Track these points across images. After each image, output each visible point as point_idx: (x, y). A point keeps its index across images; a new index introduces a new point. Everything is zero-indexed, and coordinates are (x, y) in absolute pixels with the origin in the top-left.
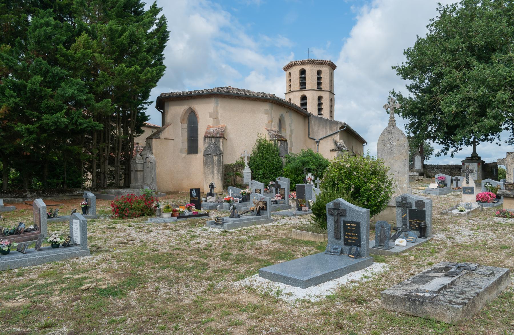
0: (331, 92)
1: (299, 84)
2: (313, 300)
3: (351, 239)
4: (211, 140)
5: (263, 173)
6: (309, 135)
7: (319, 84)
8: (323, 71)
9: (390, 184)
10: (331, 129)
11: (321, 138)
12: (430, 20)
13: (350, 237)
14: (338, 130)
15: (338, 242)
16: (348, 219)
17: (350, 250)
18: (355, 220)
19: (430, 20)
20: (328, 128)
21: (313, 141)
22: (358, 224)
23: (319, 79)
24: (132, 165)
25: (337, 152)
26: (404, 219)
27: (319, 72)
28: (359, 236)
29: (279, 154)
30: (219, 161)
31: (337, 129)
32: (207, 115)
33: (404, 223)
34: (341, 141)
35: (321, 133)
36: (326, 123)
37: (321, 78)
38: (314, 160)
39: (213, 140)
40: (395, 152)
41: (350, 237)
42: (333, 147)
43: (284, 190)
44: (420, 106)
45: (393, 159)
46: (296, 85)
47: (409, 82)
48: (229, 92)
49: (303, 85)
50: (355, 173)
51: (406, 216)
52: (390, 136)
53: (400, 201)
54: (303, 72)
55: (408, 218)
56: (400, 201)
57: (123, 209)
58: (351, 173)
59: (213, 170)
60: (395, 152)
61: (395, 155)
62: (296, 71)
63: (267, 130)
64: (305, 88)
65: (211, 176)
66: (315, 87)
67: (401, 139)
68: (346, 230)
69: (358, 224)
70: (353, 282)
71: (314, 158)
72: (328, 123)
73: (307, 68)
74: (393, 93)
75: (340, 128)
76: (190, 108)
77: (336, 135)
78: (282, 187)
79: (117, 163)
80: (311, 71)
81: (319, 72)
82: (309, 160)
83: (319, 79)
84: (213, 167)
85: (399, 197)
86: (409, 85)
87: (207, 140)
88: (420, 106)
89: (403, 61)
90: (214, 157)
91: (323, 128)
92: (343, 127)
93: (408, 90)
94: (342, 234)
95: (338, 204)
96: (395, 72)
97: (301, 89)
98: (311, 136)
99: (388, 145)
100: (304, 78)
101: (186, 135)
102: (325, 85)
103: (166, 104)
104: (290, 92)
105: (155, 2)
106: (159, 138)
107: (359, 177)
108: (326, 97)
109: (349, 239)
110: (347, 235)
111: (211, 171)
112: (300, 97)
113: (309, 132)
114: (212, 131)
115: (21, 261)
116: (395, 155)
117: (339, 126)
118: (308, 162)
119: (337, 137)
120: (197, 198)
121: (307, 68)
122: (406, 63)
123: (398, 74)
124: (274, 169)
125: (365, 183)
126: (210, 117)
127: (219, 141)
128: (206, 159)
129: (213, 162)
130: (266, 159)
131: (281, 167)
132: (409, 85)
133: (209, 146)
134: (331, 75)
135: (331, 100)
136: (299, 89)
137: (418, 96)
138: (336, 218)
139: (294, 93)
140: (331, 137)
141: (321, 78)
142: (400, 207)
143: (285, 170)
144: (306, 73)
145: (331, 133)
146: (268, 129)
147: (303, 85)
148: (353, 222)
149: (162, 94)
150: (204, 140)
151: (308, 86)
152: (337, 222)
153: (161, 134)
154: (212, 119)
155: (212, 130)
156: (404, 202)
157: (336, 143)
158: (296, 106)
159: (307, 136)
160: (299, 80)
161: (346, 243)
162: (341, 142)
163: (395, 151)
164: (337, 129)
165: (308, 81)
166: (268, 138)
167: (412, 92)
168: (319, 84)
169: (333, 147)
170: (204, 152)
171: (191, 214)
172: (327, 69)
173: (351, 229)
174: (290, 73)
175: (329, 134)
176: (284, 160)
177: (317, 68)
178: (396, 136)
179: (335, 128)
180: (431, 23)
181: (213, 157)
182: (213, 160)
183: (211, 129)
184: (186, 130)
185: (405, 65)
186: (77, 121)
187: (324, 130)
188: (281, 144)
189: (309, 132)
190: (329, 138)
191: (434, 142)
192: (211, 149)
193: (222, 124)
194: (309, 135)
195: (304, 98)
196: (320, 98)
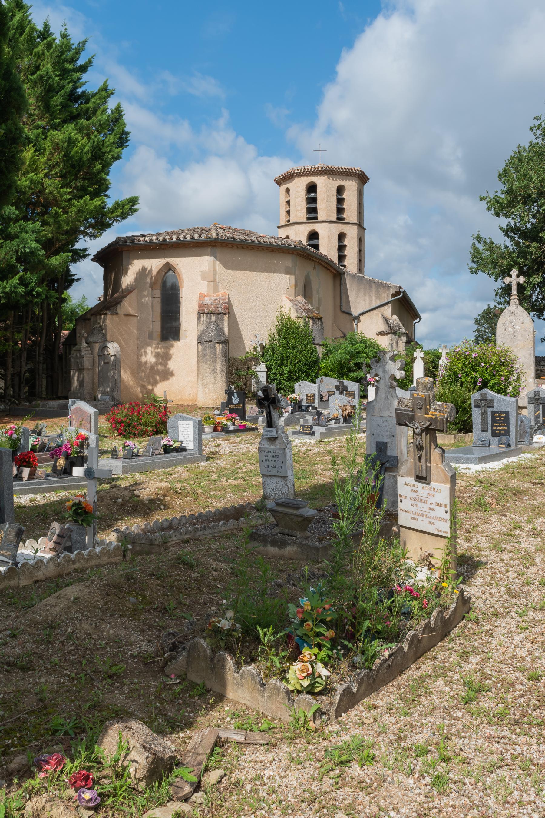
0: (360, 226)
1: (304, 211)
2: (491, 470)
3: (499, 430)
4: (210, 318)
5: (288, 372)
6: (341, 308)
7: (340, 210)
8: (347, 188)
9: (518, 377)
10: (378, 297)
11: (361, 311)
12: (536, 119)
13: (499, 428)
14: (390, 299)
15: (484, 434)
16: (495, 409)
17: (500, 440)
18: (504, 410)
19: (536, 119)
20: (373, 295)
21: (347, 316)
22: (507, 413)
23: (340, 201)
24: (72, 360)
25: (389, 336)
26: (537, 417)
27: (340, 190)
28: (508, 426)
29: (313, 339)
30: (226, 353)
31: (387, 296)
32: (196, 275)
33: (537, 422)
34: (395, 317)
35: (362, 303)
36: (370, 287)
37: (344, 199)
38: (367, 350)
39: (213, 318)
40: (519, 338)
41: (499, 428)
42: (382, 327)
43: (354, 394)
44: (522, 260)
45: (516, 347)
46: (299, 210)
47: (504, 221)
48: (233, 238)
49: (312, 212)
50: (483, 365)
51: (539, 414)
52: (512, 318)
53: (533, 396)
54: (312, 188)
55: (541, 416)
56: (533, 396)
57: (129, 425)
58: (478, 365)
59: (215, 367)
60: (519, 338)
61: (518, 342)
62: (299, 187)
63: (291, 301)
64: (316, 218)
65: (211, 376)
66: (334, 217)
67: (525, 322)
68: (494, 420)
69: (507, 413)
70: (513, 462)
71: (369, 347)
72: (373, 286)
73: (320, 181)
74: (479, 239)
75: (393, 295)
76: (168, 264)
77: (386, 307)
78: (349, 389)
79: (39, 356)
80: (326, 187)
81: (340, 190)
82: (360, 350)
83: (340, 201)
84: (215, 361)
85: (531, 392)
86: (504, 226)
87: (204, 318)
88: (522, 260)
89: (497, 189)
90: (217, 345)
91: (365, 295)
92: (398, 293)
93: (502, 234)
94: (490, 426)
95: (486, 394)
96: (484, 205)
97: (308, 219)
98: (344, 309)
99: (510, 329)
100: (314, 200)
101: (158, 308)
102: (350, 214)
103: (125, 255)
104: (289, 224)
105: (106, 82)
106: (117, 314)
107: (487, 369)
108: (352, 233)
109: (497, 430)
110: (496, 426)
111: (212, 368)
112: (306, 233)
113: (341, 302)
114: (209, 303)
115: (155, 463)
116: (518, 342)
117: (392, 291)
118: (358, 353)
119: (388, 311)
120: (241, 406)
121: (320, 181)
122: (502, 191)
123: (489, 209)
124: (305, 364)
125: (494, 375)
126: (203, 278)
127: (222, 320)
128: (204, 350)
129: (216, 353)
130: (294, 348)
131: (316, 362)
132: (504, 226)
133: (207, 327)
134: (360, 193)
135: (361, 240)
136: (305, 220)
137: (517, 244)
138: (483, 409)
139: (296, 226)
140: (378, 310)
141: (344, 199)
142: (533, 403)
143: (323, 366)
144: (319, 190)
145: (379, 303)
146: (291, 298)
147: (312, 212)
148: (502, 412)
149: (119, 238)
150: (199, 318)
151: (321, 215)
152: (484, 414)
153: (119, 306)
154: (206, 282)
155: (208, 301)
156: (537, 397)
157: (386, 320)
158: (332, 262)
159: (338, 308)
160: (304, 202)
161: (495, 435)
162: (395, 320)
163: (519, 337)
164: (388, 297)
165: (320, 205)
166: (293, 315)
167: (508, 237)
168: (340, 210)
169: (382, 327)
170: (199, 337)
171: (236, 428)
172: (354, 182)
173: (500, 420)
174: (288, 190)
175: (374, 306)
176: (321, 351)
177: (337, 182)
178: (520, 317)
179: (385, 295)
180: (537, 123)
181: (215, 346)
182: (215, 350)
183: (207, 298)
184: (158, 300)
185: (499, 194)
186: (33, 290)
187: (367, 298)
188: (314, 323)
189: (341, 302)
190: (375, 312)
191: (539, 318)
192: (211, 334)
193: (222, 292)
194: (341, 308)
195: (313, 236)
196: (341, 237)
